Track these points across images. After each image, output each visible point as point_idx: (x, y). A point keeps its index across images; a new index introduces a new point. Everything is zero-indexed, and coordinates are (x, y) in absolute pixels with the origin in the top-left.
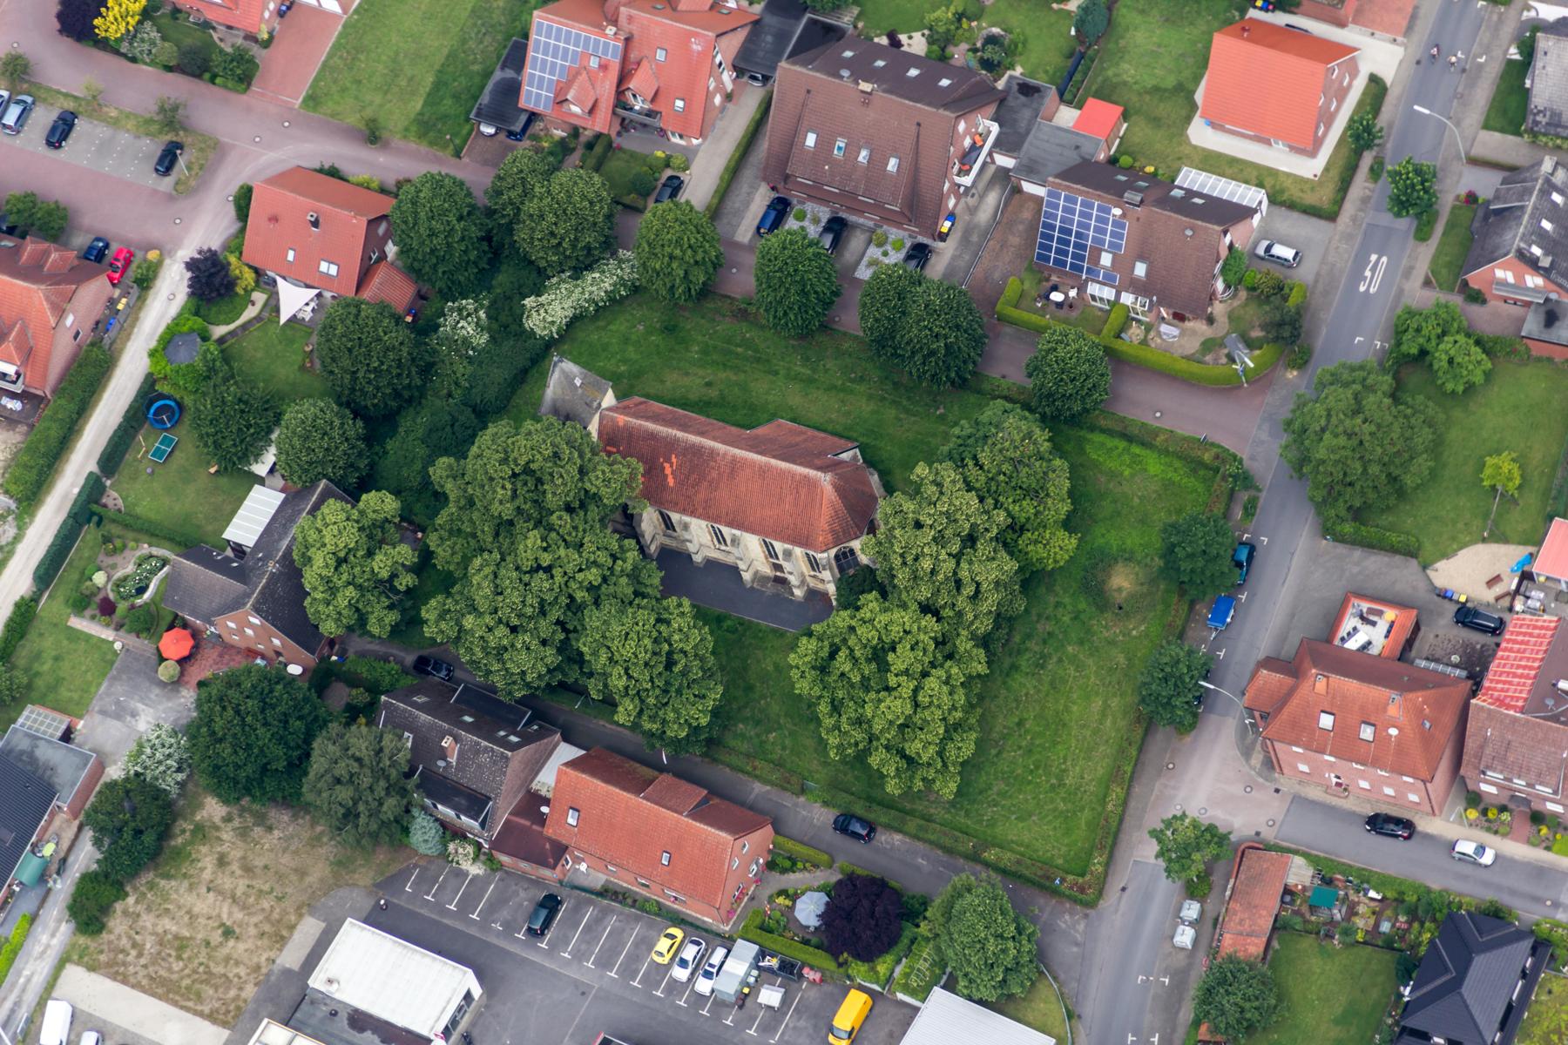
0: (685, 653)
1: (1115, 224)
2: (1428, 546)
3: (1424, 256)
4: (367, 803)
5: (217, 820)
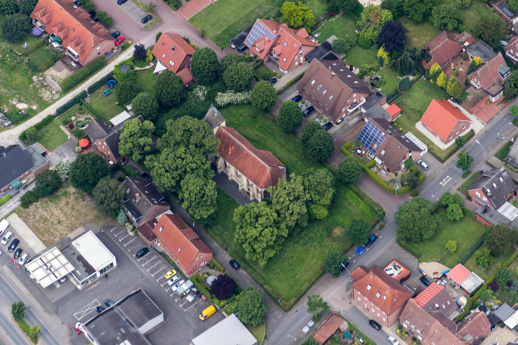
0: (208, 196)
1: (382, 137)
3: (461, 182)
5: (71, 192)
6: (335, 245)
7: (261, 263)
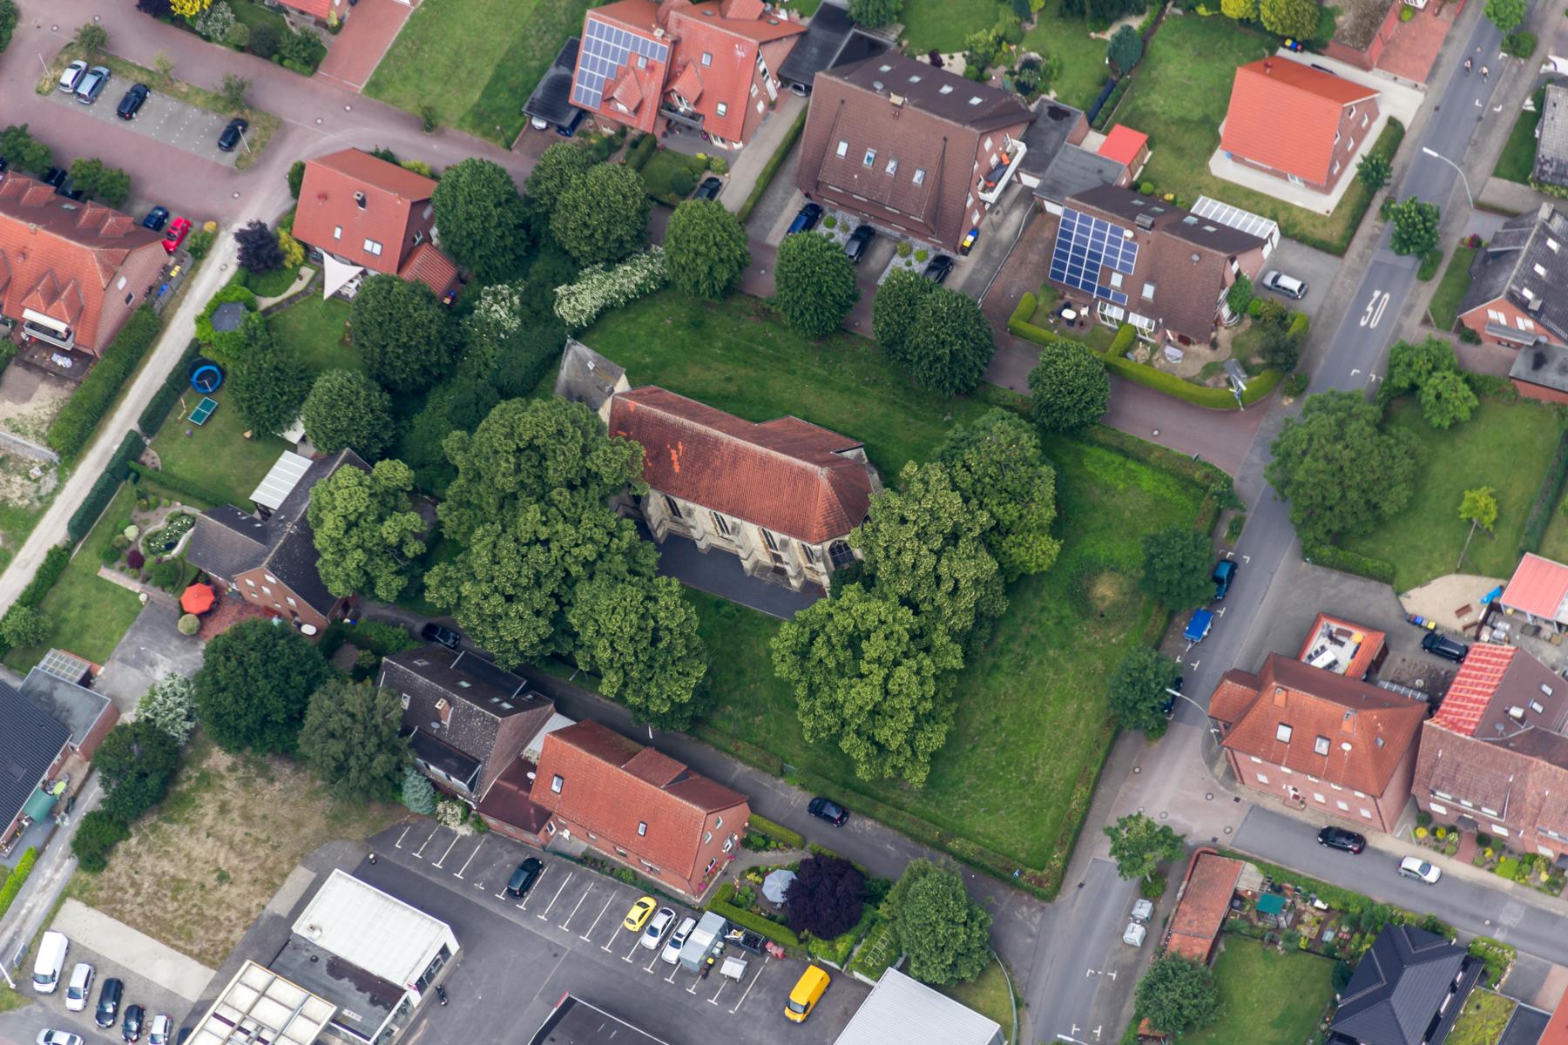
0: (671, 631)
1: (1127, 246)
2: (1403, 574)
3: (1425, 295)
4: (358, 758)
5: (222, 769)
6: (1116, 637)
7: (915, 779)
